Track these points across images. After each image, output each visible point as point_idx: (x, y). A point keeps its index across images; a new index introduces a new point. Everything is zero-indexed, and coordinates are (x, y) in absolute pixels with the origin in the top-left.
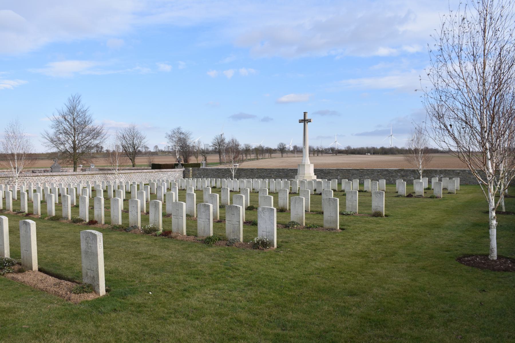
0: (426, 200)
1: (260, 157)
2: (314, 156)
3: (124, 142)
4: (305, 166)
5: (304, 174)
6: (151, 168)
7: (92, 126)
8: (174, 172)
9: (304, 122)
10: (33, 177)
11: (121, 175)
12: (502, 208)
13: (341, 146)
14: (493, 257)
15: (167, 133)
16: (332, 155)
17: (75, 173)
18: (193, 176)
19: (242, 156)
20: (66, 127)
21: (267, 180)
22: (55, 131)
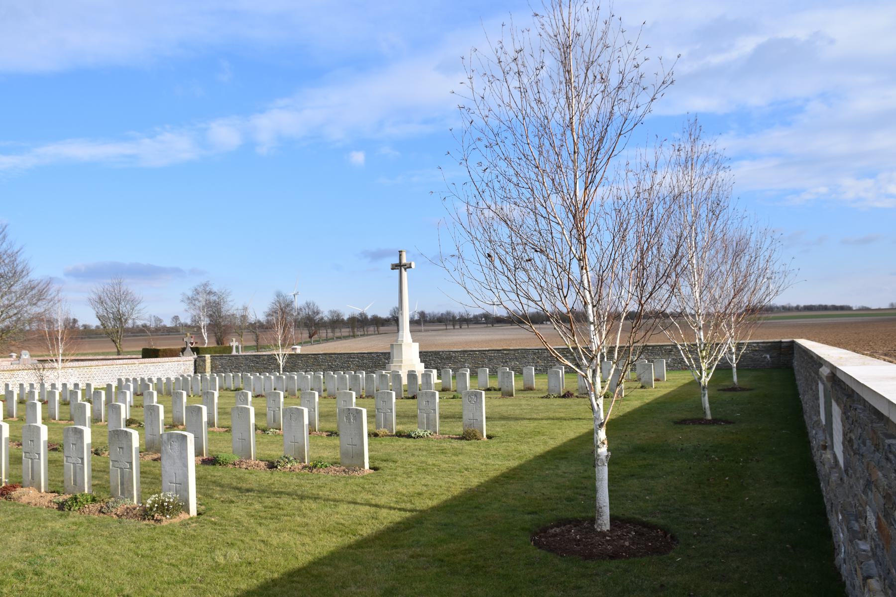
1: (359, 333)
2: (454, 329)
5: (401, 362)
6: (141, 356)
7: (30, 281)
12: (705, 412)
14: (601, 525)
16: (486, 325)
18: (212, 370)
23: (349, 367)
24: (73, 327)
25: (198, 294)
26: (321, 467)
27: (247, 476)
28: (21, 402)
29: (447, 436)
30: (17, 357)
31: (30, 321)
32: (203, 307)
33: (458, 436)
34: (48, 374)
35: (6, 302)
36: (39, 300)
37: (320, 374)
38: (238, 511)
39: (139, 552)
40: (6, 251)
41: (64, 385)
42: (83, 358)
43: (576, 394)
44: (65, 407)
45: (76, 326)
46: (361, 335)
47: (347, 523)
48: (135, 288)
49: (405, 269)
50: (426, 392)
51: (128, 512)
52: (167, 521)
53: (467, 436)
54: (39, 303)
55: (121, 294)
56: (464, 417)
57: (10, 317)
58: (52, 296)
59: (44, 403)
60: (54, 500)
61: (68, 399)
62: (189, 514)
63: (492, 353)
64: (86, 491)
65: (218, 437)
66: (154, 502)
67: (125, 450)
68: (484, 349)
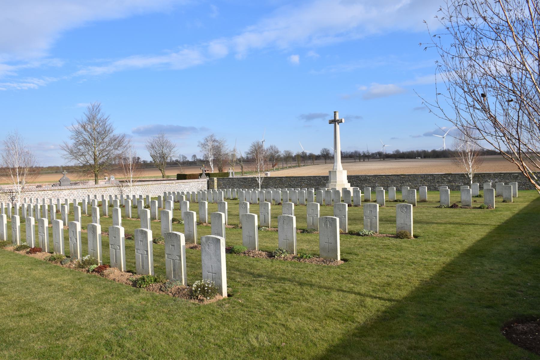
0: (474, 211)
1: (302, 164)
2: (360, 161)
3: (153, 152)
5: (336, 182)
6: (176, 179)
8: (197, 183)
9: (334, 122)
10: (39, 192)
13: (389, 150)
15: (199, 142)
16: (379, 159)
17: (96, 186)
18: (218, 187)
20: (87, 138)
22: (75, 142)
23: (301, 185)
24: (138, 162)
25: (208, 141)
26: (306, 258)
27: (255, 263)
28: (111, 206)
29: (385, 235)
30: (108, 179)
31: (115, 159)
32: (211, 149)
33: (393, 235)
34: (125, 189)
35: (101, 148)
36: (119, 146)
37: (280, 190)
38: (257, 295)
39: (191, 331)
40: (100, 119)
41: (134, 196)
42: (143, 180)
43: (460, 206)
44: (135, 209)
45: (139, 161)
46: (303, 166)
47: (344, 310)
48: (172, 139)
49: (338, 123)
50: (370, 204)
51: (179, 291)
52: (208, 301)
53: (401, 235)
54: (119, 148)
55: (164, 142)
56: (397, 222)
57: (104, 156)
58: (126, 144)
59: (122, 206)
60: (130, 279)
61: (136, 205)
62: (222, 295)
63: (394, 177)
64: (150, 274)
65: (229, 232)
66: (198, 287)
67: (175, 246)
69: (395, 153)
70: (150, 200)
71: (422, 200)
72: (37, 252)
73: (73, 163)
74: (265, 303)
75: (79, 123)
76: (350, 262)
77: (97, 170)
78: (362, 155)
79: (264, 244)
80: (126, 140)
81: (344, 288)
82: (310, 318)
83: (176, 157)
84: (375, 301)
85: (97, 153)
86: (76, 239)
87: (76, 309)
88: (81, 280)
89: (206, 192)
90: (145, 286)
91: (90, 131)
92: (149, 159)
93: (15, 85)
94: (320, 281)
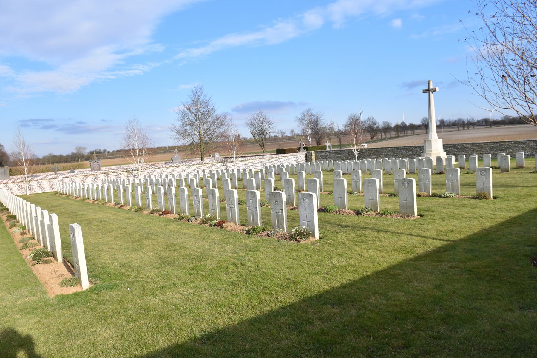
1: (401, 135)
2: (464, 130)
4: (432, 142)
5: (431, 151)
6: (276, 153)
10: (155, 169)
11: (240, 162)
16: (486, 127)
17: (203, 162)
19: (381, 135)
21: (375, 160)
25: (305, 116)
27: (344, 218)
29: (465, 197)
30: (213, 156)
33: (473, 197)
34: (229, 165)
35: (206, 127)
36: (221, 125)
39: (291, 257)
41: (239, 170)
42: (245, 155)
46: (403, 136)
47: (407, 247)
48: (270, 115)
49: (432, 92)
51: (282, 236)
52: (303, 242)
54: (221, 127)
56: (477, 185)
57: (208, 135)
62: (315, 238)
63: (492, 144)
64: (259, 225)
67: (278, 203)
68: (487, 142)
69: (504, 119)
70: (253, 173)
71: (519, 167)
72: (168, 214)
73: (181, 143)
74: (347, 242)
75: (185, 106)
76: (424, 217)
77: (203, 148)
78: (466, 122)
79: (354, 205)
80: (227, 119)
81: (413, 234)
82: (380, 251)
83: (275, 133)
84: (435, 241)
85: (202, 133)
86: (199, 202)
87: (207, 247)
88: (207, 231)
89: (304, 165)
90: (255, 233)
91: (195, 112)
92: (249, 136)
93: (123, 73)
94: (394, 229)
